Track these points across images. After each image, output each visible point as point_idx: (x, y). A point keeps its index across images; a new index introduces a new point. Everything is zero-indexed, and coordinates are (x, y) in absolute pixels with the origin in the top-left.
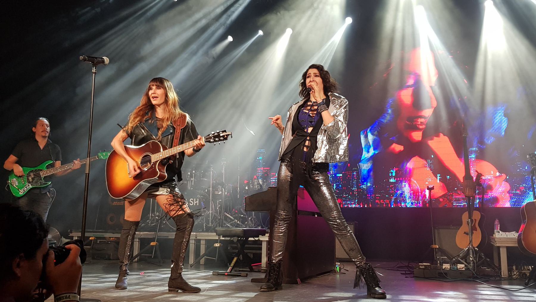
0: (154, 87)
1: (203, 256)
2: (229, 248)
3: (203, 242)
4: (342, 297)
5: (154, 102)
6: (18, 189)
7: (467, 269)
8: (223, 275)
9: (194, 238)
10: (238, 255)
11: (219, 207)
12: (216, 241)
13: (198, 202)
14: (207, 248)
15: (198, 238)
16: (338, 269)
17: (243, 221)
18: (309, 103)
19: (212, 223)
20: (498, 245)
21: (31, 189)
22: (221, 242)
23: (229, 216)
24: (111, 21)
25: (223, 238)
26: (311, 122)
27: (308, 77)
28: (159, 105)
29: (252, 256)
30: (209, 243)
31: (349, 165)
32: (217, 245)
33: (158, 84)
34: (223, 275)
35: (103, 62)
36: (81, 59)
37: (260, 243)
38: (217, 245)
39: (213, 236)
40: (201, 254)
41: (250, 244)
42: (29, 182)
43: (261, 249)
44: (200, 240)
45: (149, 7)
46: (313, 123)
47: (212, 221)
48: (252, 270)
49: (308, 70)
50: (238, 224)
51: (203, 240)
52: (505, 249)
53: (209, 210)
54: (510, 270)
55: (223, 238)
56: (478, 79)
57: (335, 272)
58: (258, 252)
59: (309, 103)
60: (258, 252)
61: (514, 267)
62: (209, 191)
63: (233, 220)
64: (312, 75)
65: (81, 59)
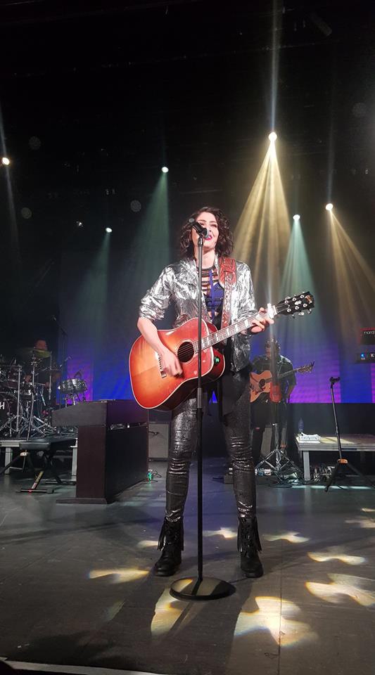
1: (8, 466)
3: (8, 450)
4: (23, 670)
7: (273, 474)
13: (3, 406)
16: (150, 477)
19: (20, 427)
20: (301, 449)
23: (40, 420)
24: (289, 274)
32: (24, 454)
38: (24, 454)
40: (6, 464)
43: (71, 454)
45: (289, 274)
52: (308, 453)
53: (16, 414)
54: (312, 472)
56: (285, 276)
57: (147, 480)
61: (316, 471)
63: (42, 424)
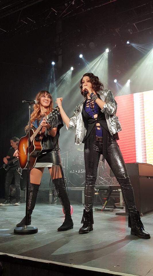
8: (100, 210)
10: (107, 200)
17: (109, 180)
18: (88, 101)
26: (94, 111)
27: (83, 83)
29: (114, 199)
31: (11, 148)
34: (100, 210)
36: (23, 102)
37: (119, 192)
41: (114, 193)
43: (119, 195)
48: (115, 207)
49: (83, 78)
50: (106, 182)
58: (118, 197)
59: (88, 101)
60: (118, 197)
64: (86, 82)
65: (23, 102)
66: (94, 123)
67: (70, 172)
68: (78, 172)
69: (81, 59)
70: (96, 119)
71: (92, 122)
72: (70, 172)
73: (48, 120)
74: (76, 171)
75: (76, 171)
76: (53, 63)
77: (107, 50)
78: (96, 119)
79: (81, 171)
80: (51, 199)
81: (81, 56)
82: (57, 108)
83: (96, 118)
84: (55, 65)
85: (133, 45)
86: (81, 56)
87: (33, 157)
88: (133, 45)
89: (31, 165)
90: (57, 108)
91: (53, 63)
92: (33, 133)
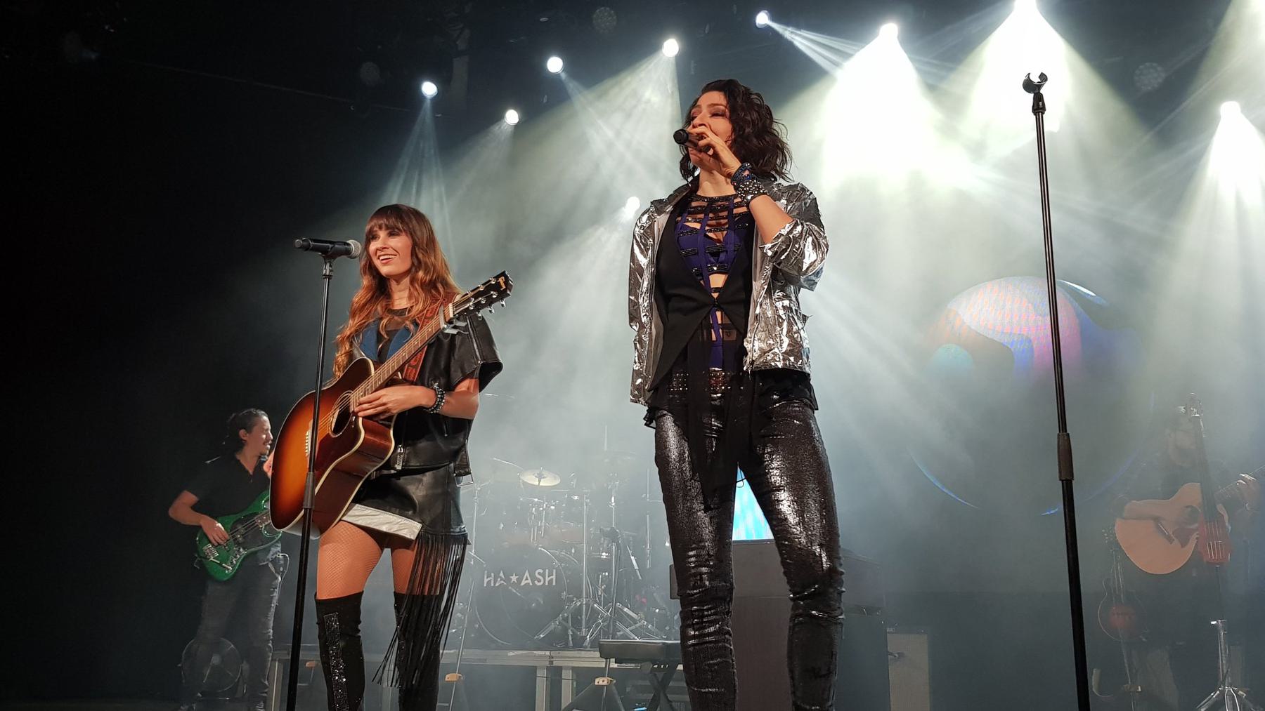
0: (382, 234)
2: (628, 690)
3: (567, 674)
5: (384, 270)
6: (220, 564)
9: (547, 664)
11: (604, 591)
12: (600, 672)
13: (554, 577)
14: (576, 691)
15: (555, 664)
21: (246, 557)
22: (612, 673)
25: (616, 666)
28: (398, 278)
30: (584, 676)
33: (392, 221)
35: (347, 252)
38: (600, 681)
39: (593, 659)
42: (239, 544)
44: (560, 669)
46: (722, 256)
47: (587, 622)
50: (650, 631)
51: (567, 668)
55: (616, 666)
62: (579, 551)
66: (707, 309)
67: (486, 580)
68: (519, 580)
69: (422, 97)
70: (715, 295)
71: (692, 304)
72: (486, 580)
73: (450, 322)
74: (514, 578)
75: (514, 578)
76: (429, 89)
77: (671, 47)
78: (715, 295)
79: (533, 578)
80: (744, 209)
81: (555, 64)
82: (501, 280)
83: (717, 290)
84: (435, 99)
85: (788, 33)
86: (555, 64)
87: (346, 475)
88: (788, 33)
89: (323, 516)
90: (501, 280)
91: (429, 89)
92: (367, 374)
